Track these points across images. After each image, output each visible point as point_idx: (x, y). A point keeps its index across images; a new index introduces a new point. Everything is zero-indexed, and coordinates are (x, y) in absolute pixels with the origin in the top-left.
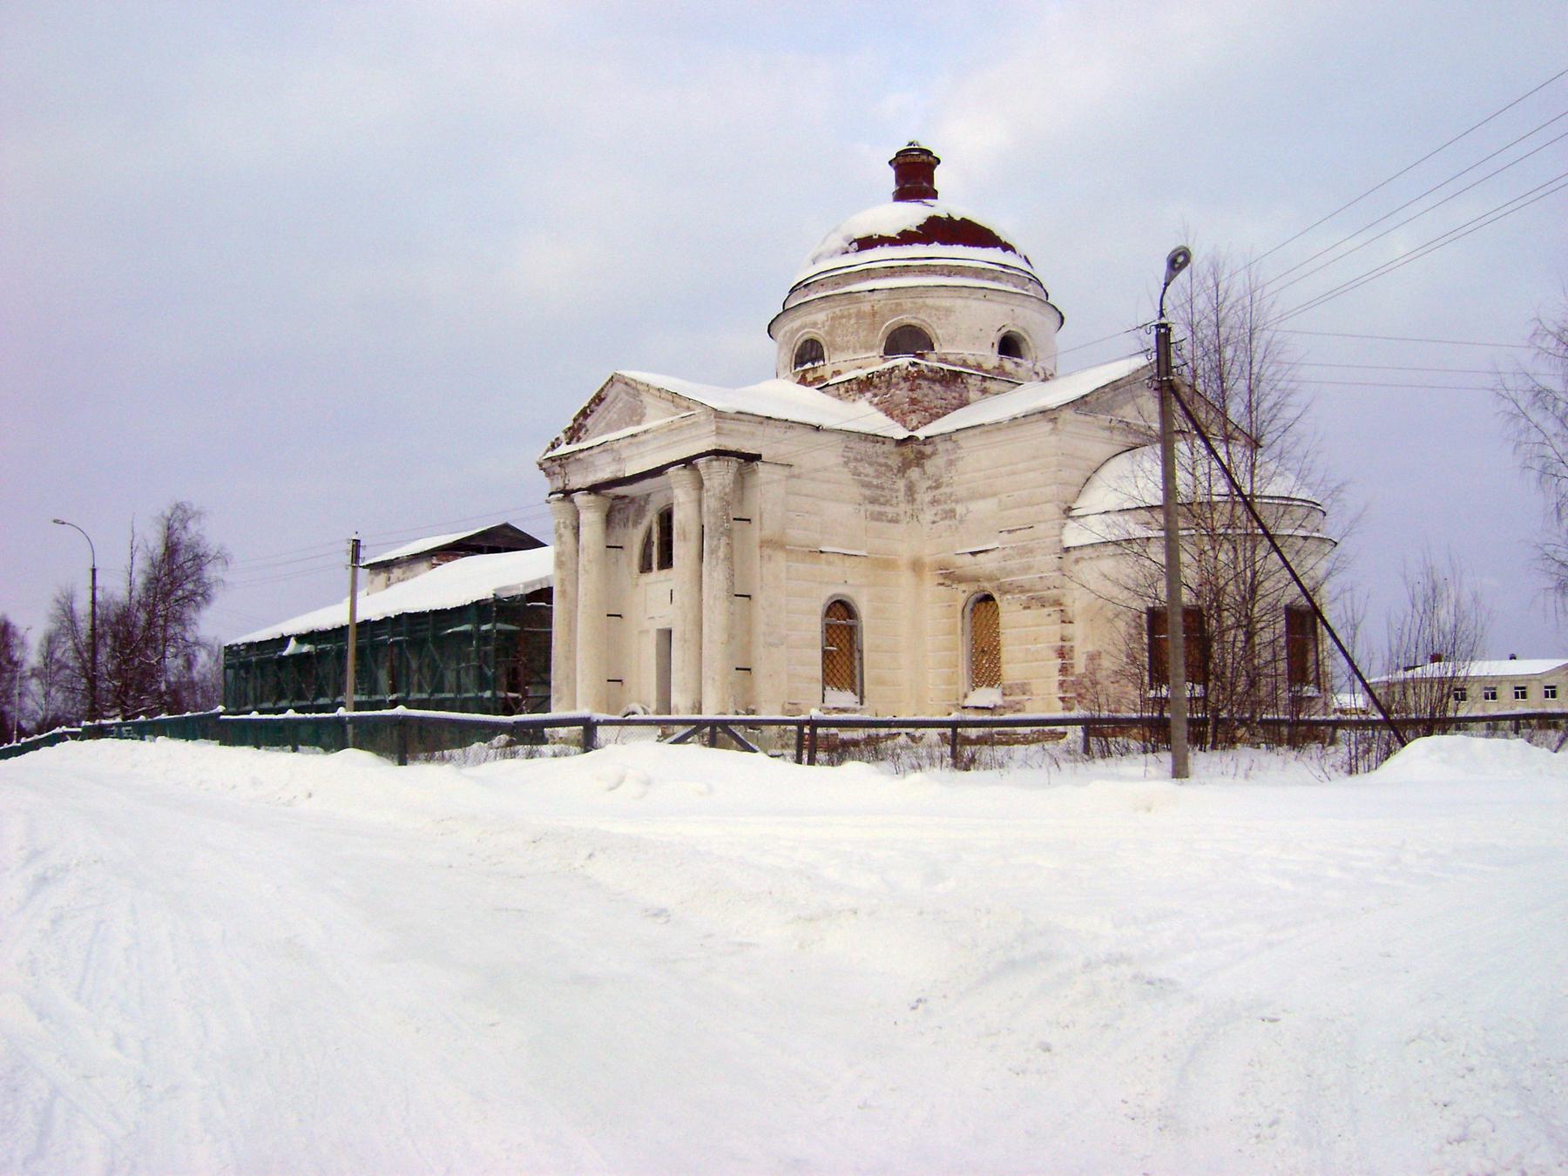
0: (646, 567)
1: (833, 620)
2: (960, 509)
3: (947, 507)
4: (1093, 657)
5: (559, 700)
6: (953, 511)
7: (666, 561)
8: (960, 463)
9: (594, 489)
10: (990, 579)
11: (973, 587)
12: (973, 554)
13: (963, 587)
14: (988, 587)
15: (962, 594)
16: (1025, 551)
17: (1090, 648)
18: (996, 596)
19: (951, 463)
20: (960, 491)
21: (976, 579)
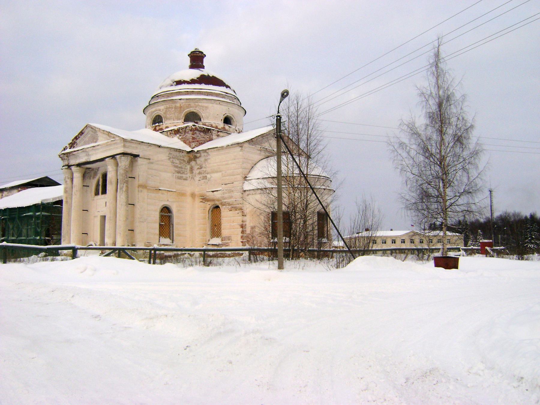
0: (97, 194)
1: (163, 214)
2: (208, 176)
3: (204, 175)
4: (253, 228)
5: (64, 240)
6: (206, 177)
7: (104, 192)
8: (209, 161)
9: (79, 165)
10: (218, 200)
11: (212, 203)
12: (213, 192)
13: (209, 203)
14: (218, 203)
15: (208, 206)
16: (231, 191)
17: (252, 225)
18: (220, 206)
19: (206, 160)
20: (209, 170)
21: (213, 200)
